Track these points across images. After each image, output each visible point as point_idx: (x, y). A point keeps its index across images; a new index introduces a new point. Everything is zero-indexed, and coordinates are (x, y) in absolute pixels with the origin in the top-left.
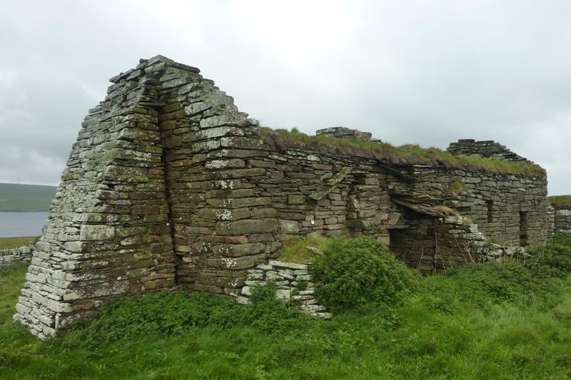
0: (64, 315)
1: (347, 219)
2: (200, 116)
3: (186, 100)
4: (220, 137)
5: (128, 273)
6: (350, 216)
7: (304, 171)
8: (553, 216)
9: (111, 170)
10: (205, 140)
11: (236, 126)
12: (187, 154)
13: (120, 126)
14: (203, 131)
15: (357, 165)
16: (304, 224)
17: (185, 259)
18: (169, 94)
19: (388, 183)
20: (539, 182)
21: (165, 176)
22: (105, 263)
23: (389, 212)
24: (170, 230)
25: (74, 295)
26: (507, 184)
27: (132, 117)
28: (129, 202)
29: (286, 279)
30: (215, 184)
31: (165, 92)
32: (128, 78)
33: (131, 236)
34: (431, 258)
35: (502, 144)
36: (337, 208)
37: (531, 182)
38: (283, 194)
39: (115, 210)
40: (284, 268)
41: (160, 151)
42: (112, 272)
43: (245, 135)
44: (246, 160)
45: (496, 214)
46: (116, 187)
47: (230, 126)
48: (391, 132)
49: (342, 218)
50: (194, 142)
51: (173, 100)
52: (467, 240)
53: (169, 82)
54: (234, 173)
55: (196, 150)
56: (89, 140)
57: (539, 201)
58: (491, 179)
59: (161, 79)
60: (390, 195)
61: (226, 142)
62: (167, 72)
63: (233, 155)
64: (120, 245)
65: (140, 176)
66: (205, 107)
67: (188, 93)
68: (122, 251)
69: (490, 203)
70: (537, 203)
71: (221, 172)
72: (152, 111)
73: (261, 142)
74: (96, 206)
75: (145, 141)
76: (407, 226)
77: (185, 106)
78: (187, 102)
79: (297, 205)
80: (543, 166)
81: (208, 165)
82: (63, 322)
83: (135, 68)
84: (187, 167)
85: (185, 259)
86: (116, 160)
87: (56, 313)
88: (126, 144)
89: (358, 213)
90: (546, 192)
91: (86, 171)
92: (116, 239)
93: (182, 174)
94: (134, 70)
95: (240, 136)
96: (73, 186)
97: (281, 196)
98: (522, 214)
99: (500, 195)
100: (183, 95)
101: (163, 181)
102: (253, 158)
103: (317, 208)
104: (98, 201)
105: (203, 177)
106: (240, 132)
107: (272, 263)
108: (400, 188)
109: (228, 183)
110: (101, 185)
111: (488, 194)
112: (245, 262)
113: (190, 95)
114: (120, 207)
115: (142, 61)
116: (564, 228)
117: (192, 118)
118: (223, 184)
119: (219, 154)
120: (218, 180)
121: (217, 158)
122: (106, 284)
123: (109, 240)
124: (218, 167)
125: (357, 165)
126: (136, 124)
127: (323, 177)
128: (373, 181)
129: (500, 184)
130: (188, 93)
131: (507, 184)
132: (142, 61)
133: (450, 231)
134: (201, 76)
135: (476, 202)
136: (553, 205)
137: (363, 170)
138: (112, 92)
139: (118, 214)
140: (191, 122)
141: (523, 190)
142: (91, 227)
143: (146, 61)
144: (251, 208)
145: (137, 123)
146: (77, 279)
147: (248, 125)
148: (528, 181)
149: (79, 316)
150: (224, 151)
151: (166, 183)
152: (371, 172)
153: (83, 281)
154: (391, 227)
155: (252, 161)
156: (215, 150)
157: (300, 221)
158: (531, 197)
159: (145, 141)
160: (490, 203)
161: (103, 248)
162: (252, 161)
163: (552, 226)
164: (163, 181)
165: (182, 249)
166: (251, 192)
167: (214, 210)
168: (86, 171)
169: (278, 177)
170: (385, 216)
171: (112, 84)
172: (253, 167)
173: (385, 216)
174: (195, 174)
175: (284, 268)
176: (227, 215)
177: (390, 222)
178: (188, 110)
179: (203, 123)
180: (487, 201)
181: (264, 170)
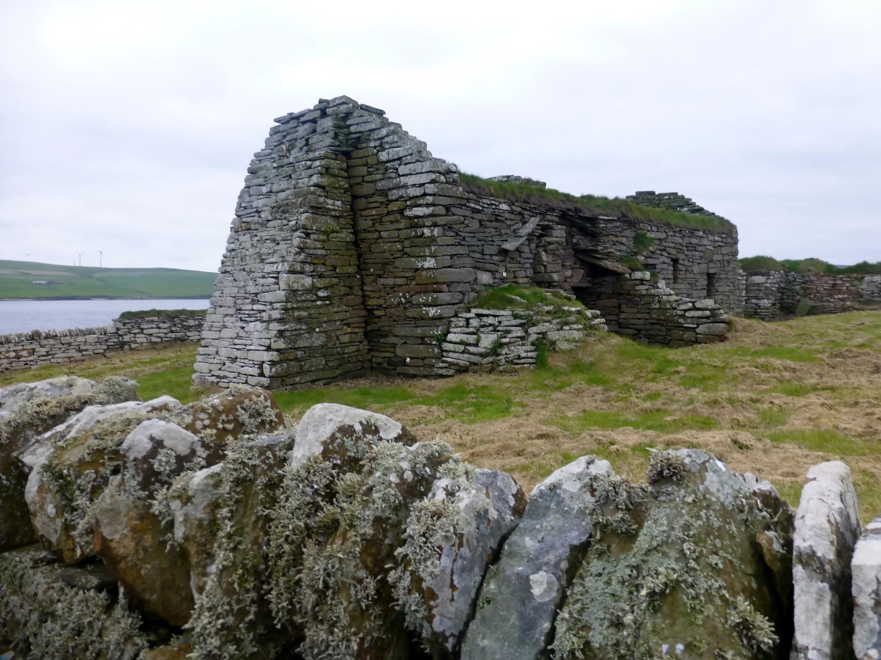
0: (273, 363)
1: (535, 273)
2: (399, 162)
3: (381, 145)
4: (424, 184)
5: (324, 325)
6: (539, 270)
7: (497, 220)
8: (744, 282)
9: (307, 218)
10: (405, 186)
11: (439, 172)
12: (382, 203)
13: (310, 172)
14: (402, 178)
15: (543, 214)
16: (497, 275)
17: (376, 313)
18: (359, 138)
19: (573, 236)
20: (729, 240)
21: (354, 226)
22: (305, 314)
23: (572, 269)
24: (360, 283)
25: (281, 344)
26: (694, 241)
27: (324, 162)
28: (323, 252)
29: (490, 325)
30: (416, 233)
31: (354, 136)
32: (302, 119)
33: (326, 288)
34: (615, 318)
35: (687, 197)
36: (526, 261)
37: (720, 239)
38: (479, 243)
39: (313, 260)
40: (487, 316)
41: (349, 198)
42: (311, 324)
43: (447, 182)
44: (447, 208)
45: (682, 275)
46: (312, 236)
47: (434, 172)
48: (571, 181)
49: (530, 273)
50: (390, 189)
51: (364, 145)
52: (653, 296)
53: (356, 126)
54: (439, 220)
55: (394, 198)
56: (264, 187)
57: (729, 262)
58: (677, 235)
59: (348, 123)
60: (574, 250)
61: (430, 189)
62: (355, 114)
63: (437, 202)
64: (317, 295)
65: (332, 224)
66: (405, 153)
67: (383, 138)
68: (319, 303)
69: (675, 261)
70: (726, 264)
71: (425, 220)
72: (340, 157)
73: (461, 189)
74: (295, 255)
75: (336, 188)
76: (590, 285)
77: (378, 151)
78: (382, 148)
79: (491, 255)
80: (733, 221)
81: (408, 213)
82: (274, 370)
83: (312, 108)
84: (381, 216)
85: (376, 313)
86: (312, 207)
87: (263, 362)
88: (319, 191)
89: (545, 266)
90: (736, 253)
91: (268, 221)
92: (314, 289)
93: (374, 224)
94: (310, 111)
95: (443, 183)
96: (252, 237)
97: (478, 246)
98: (710, 277)
99: (686, 253)
100: (376, 140)
101: (352, 230)
102: (454, 206)
103: (508, 259)
104: (298, 250)
105: (401, 226)
106: (442, 178)
107: (474, 311)
108: (584, 243)
109: (432, 231)
110: (298, 233)
111: (674, 252)
112: (448, 311)
113: (386, 140)
114: (316, 256)
115: (321, 101)
116: (757, 298)
117: (389, 165)
118: (427, 232)
119: (421, 201)
120: (421, 227)
121: (420, 206)
122: (307, 335)
123: (307, 290)
124: (421, 214)
125: (543, 214)
126: (327, 171)
127: (513, 228)
128: (559, 233)
129: (686, 240)
130: (383, 138)
131: (694, 241)
132: (321, 101)
133: (637, 288)
134: (387, 119)
135: (662, 259)
136: (744, 268)
137: (550, 221)
138: (275, 133)
139: (314, 264)
140: (386, 169)
141: (711, 248)
142: (292, 276)
143: (327, 101)
144: (452, 256)
145: (327, 169)
146: (283, 328)
147: (449, 172)
148: (717, 238)
149: (285, 365)
150: (428, 197)
151: (356, 233)
152: (558, 224)
153: (287, 330)
154: (576, 285)
155: (453, 209)
156: (417, 197)
157: (493, 272)
158: (719, 257)
159: (336, 188)
160: (675, 261)
161: (303, 298)
162: (453, 209)
163: (744, 294)
164: (352, 230)
165: (372, 302)
166: (451, 241)
167: (413, 259)
168: (268, 221)
169: (475, 225)
170: (569, 273)
171: (277, 124)
172: (454, 215)
173: (569, 273)
174: (392, 222)
175: (487, 316)
176: (430, 263)
177: (573, 280)
178: (383, 156)
179: (402, 170)
180: (672, 260)
181: (462, 218)
